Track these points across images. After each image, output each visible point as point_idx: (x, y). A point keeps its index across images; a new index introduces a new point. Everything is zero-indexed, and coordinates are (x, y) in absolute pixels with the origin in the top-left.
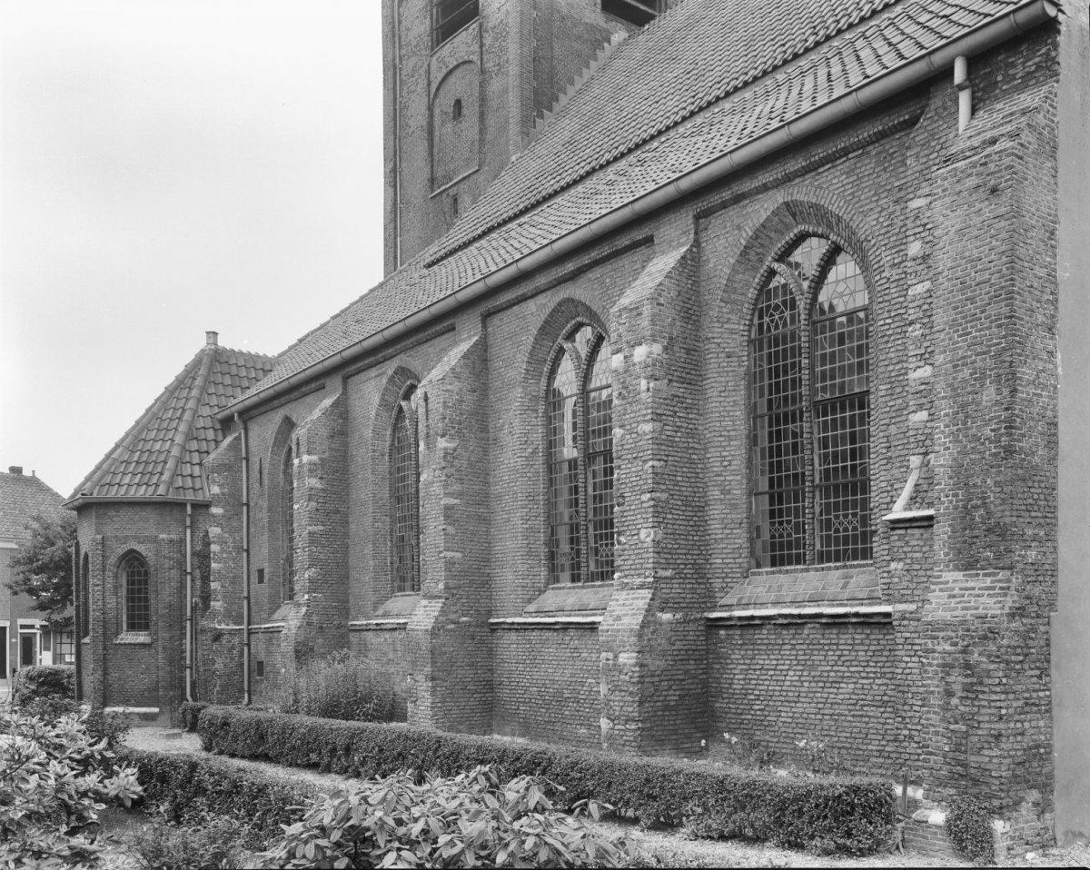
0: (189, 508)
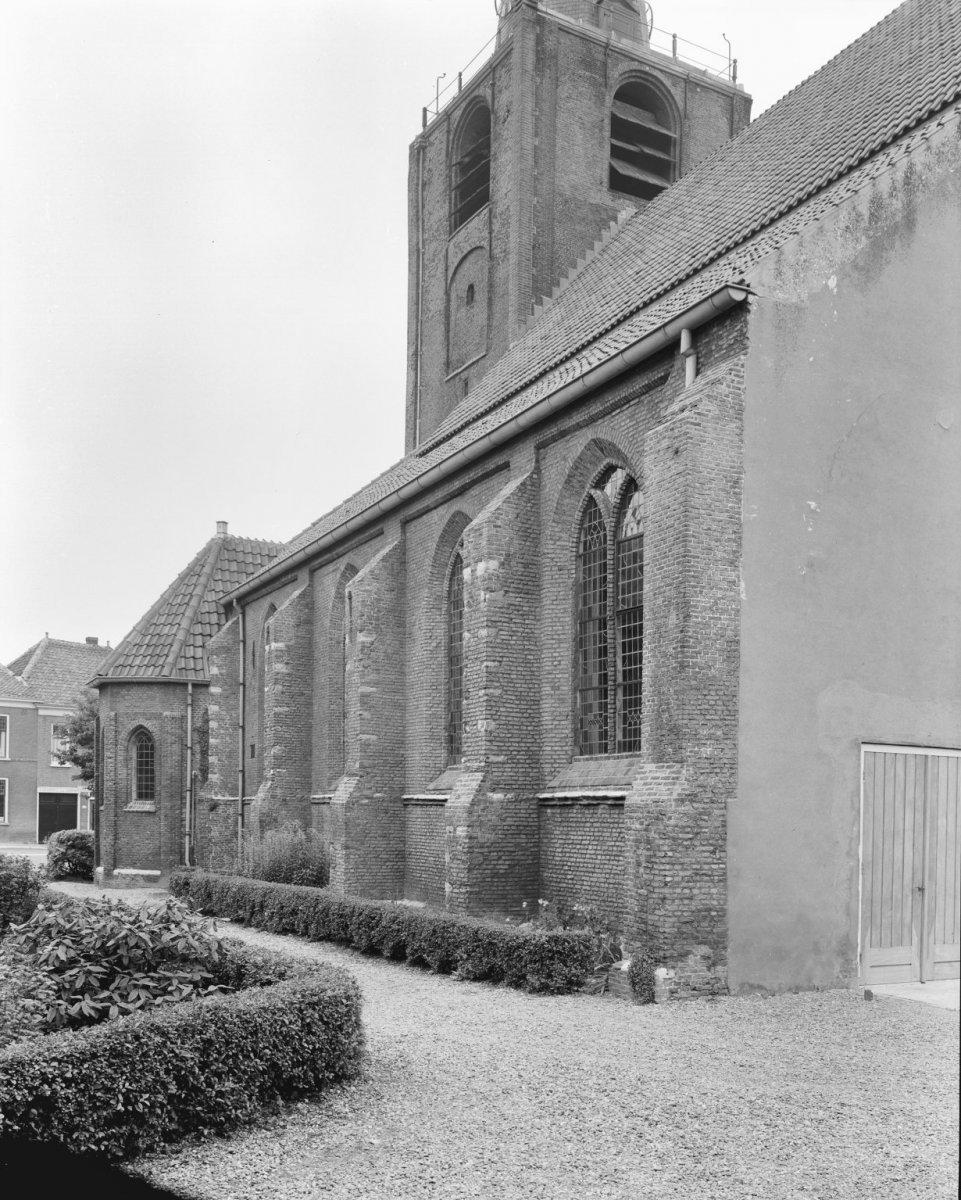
0: (190, 687)
